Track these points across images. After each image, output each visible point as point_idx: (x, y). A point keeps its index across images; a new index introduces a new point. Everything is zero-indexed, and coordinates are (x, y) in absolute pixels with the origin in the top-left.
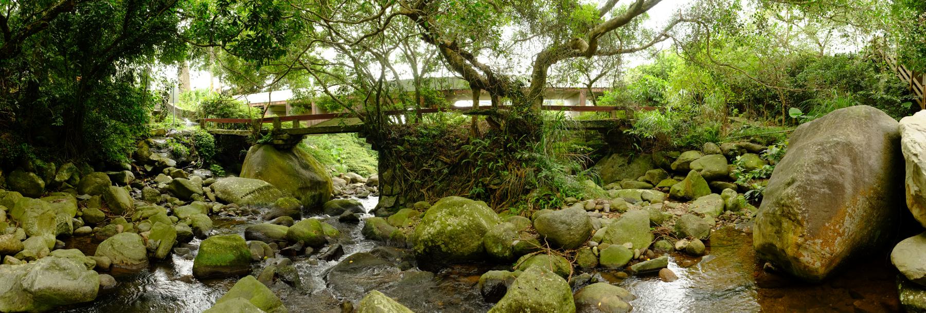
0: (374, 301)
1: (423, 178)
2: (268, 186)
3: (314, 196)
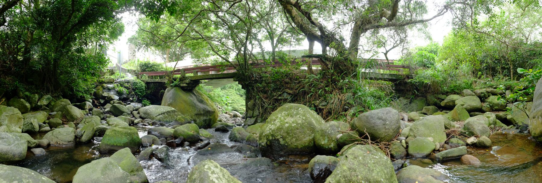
0: (204, 166)
1: (274, 104)
2: (174, 111)
3: (206, 120)
